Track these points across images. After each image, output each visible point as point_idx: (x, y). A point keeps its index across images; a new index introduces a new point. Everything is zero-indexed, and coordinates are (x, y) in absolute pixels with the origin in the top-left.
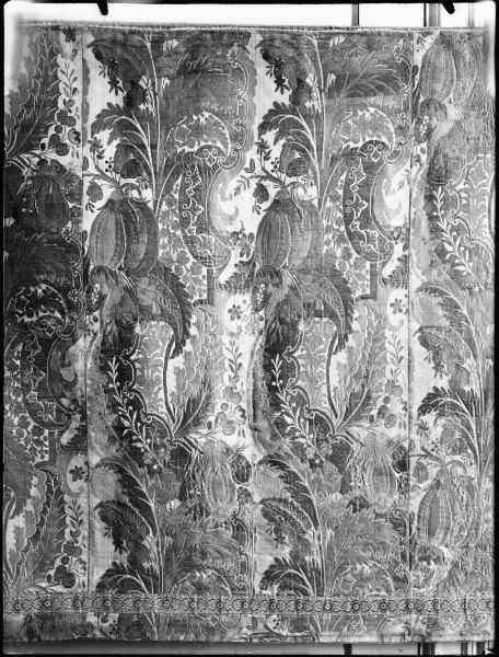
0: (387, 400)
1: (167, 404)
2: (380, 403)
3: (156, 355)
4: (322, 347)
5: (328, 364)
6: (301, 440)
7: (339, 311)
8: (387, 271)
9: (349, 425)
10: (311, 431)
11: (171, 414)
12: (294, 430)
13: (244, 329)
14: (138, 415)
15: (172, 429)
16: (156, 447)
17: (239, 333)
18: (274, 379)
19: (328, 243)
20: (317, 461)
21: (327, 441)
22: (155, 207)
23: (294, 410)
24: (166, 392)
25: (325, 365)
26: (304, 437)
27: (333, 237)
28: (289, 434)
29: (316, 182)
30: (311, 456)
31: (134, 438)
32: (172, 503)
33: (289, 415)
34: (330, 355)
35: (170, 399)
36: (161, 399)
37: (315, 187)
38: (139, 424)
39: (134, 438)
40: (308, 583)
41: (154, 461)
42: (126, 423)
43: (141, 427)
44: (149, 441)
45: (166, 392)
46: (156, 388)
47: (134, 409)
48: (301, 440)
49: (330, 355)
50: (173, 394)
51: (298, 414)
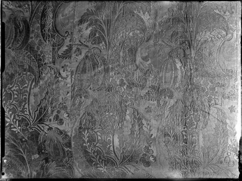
3: (26, 87)
4: (26, 85)
6: (14, 130)
7: (36, 69)
8: (60, 53)
10: (19, 125)
14: (14, 116)
15: (31, 122)
17: (67, 77)
19: (32, 38)
20: (24, 140)
21: (28, 130)
22: (30, 21)
25: (27, 94)
26: (16, 128)
27: (35, 36)
29: (29, 10)
32: (35, 156)
34: (30, 90)
35: (30, 108)
37: (28, 12)
43: (16, 122)
45: (29, 105)
47: (12, 113)
48: (14, 130)
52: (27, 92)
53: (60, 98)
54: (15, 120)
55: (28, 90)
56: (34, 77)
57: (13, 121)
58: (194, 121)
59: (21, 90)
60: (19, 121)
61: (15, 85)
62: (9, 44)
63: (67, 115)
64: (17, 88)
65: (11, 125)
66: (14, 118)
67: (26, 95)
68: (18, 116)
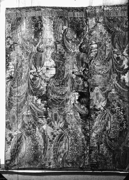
0: (53, 139)
1: (26, 140)
2: (55, 138)
3: (113, 130)
4: (112, 131)
5: (68, 149)
9: (21, 133)
10: (116, 110)
11: (110, 116)
12: (120, 110)
13: (48, 160)
16: (29, 129)
18: (125, 123)
23: (120, 115)
24: (111, 121)
28: (122, 110)
30: (116, 103)
31: (119, 109)
33: (122, 114)
34: (68, 151)
36: (112, 119)
38: (118, 113)
39: (119, 109)
40: (32, 90)
41: (30, 125)
42: (122, 113)
44: (31, 131)
46: (28, 144)
49: (68, 151)
50: (109, 120)
51: (119, 114)
52: (70, 150)
53: (53, 146)
54: (118, 113)
55: (111, 129)
56: (109, 135)
57: (119, 112)
58: (64, 79)
59: (115, 128)
60: (116, 113)
61: (75, 154)
62: (122, 153)
63: (49, 137)
64: (75, 152)
65: (120, 110)
66: (118, 114)
67: (70, 148)
68: (116, 115)
